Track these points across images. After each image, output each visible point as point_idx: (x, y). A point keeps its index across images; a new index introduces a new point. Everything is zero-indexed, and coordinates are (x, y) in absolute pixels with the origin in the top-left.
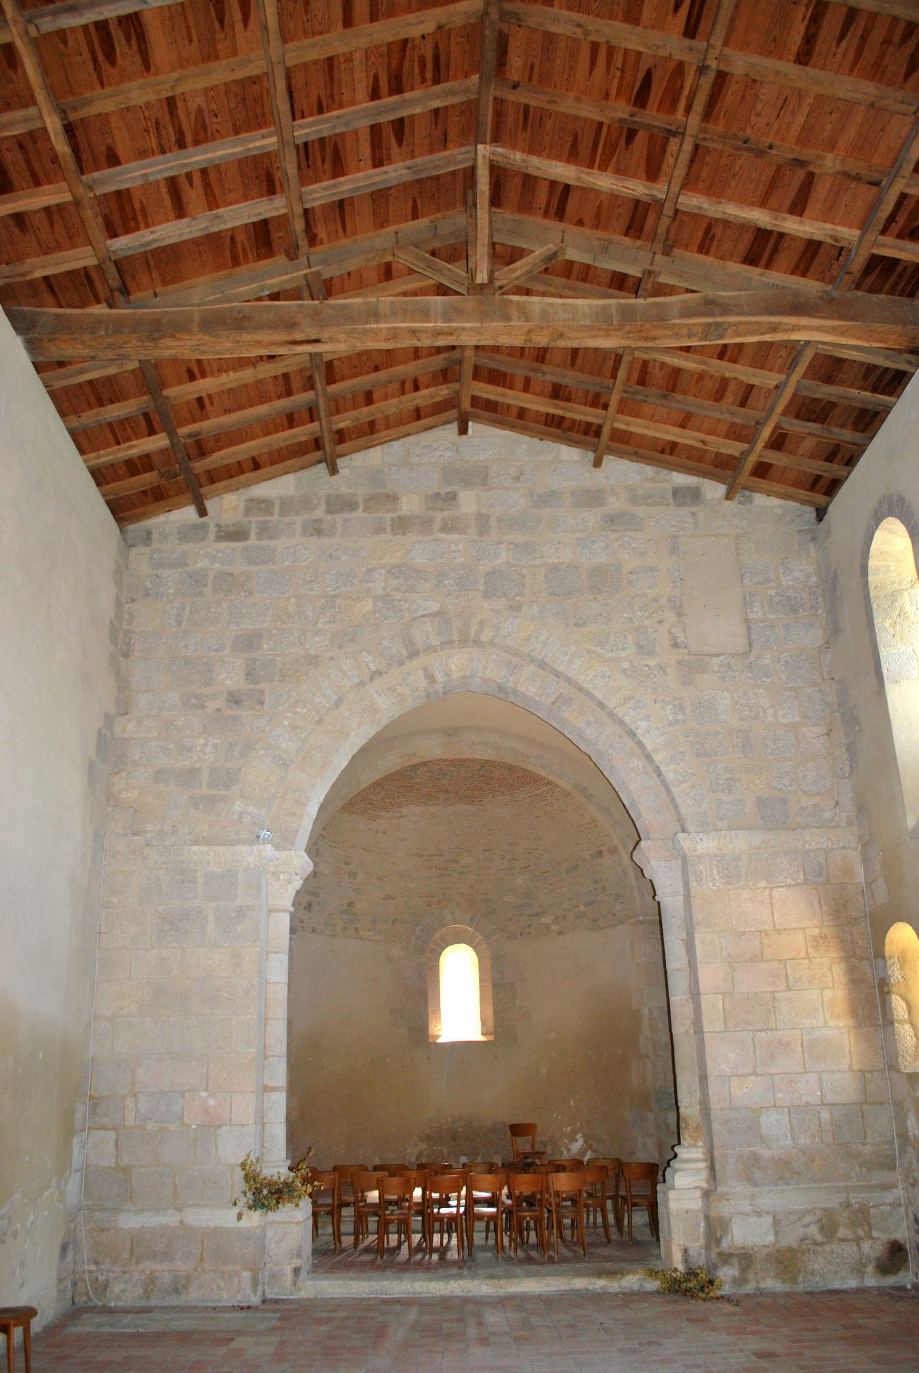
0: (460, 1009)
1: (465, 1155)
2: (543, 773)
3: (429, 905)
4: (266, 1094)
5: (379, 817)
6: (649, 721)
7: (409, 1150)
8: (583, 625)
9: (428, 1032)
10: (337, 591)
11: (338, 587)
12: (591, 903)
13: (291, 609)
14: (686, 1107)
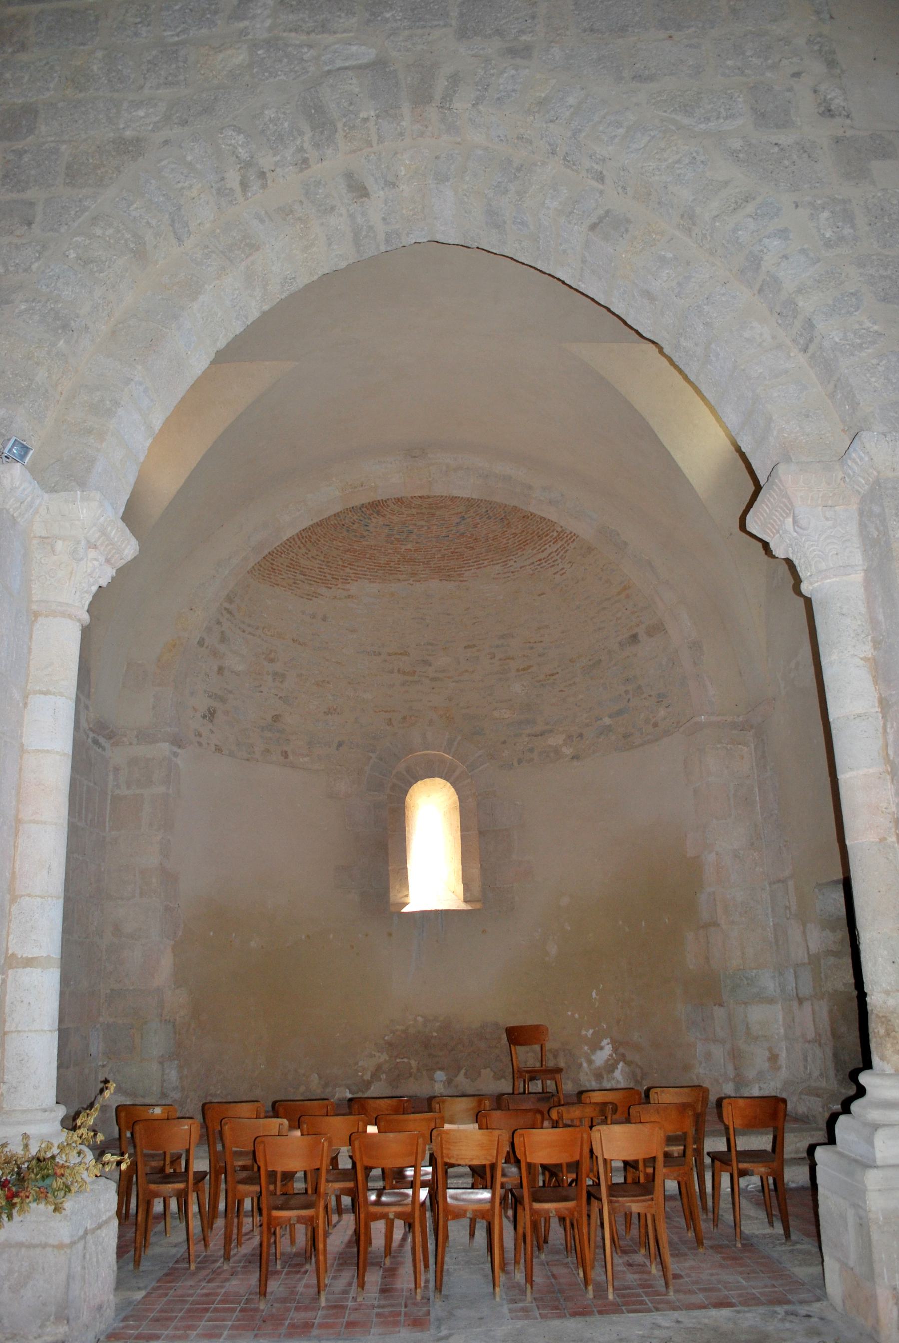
0: (433, 871)
1: (442, 1069)
2: (551, 514)
3: (389, 722)
4: (11, 972)
5: (316, 595)
6: (786, 239)
7: (360, 1064)
8: (651, 78)
9: (388, 897)
10: (182, 37)
11: (184, 31)
12: (620, 713)
13: (95, 68)
14: (887, 993)
